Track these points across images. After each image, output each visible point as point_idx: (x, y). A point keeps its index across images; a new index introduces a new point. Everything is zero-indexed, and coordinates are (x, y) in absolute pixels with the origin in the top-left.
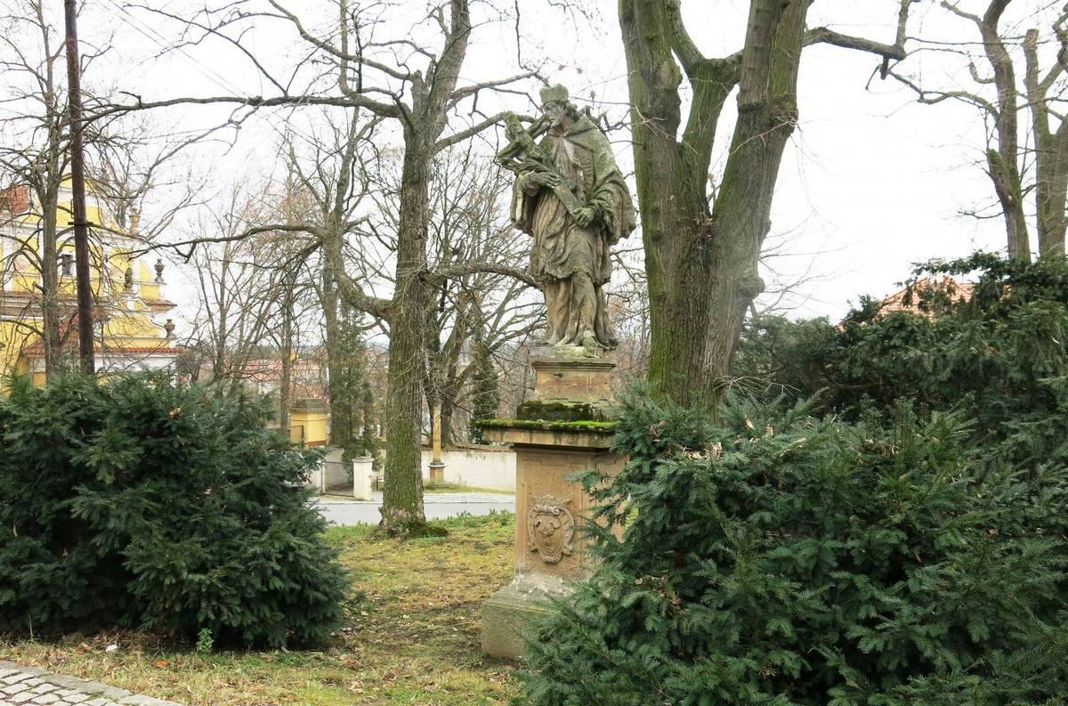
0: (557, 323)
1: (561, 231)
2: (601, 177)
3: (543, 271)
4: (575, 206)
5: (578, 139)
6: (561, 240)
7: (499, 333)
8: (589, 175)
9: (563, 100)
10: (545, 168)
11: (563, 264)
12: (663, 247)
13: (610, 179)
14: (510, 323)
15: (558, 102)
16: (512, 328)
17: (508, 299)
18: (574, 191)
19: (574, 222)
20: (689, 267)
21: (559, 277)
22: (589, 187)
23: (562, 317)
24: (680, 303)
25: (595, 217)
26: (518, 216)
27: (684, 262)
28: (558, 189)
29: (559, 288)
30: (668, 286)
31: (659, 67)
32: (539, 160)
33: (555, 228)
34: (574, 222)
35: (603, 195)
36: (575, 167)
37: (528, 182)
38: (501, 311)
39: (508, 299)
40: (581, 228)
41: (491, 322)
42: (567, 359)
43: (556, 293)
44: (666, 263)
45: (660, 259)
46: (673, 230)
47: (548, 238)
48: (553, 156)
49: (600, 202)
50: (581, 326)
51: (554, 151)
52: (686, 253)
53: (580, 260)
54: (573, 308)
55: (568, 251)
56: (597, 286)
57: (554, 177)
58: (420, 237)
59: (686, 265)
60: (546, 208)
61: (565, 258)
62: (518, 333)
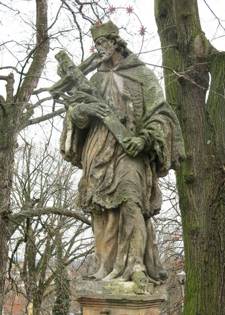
0: (105, 255)
1: (110, 162)
2: (150, 108)
3: (91, 200)
4: (125, 135)
5: (128, 73)
6: (110, 170)
7: (71, 255)
8: (138, 107)
9: (113, 34)
10: (95, 99)
11: (111, 194)
12: (196, 189)
13: (160, 110)
14: (78, 248)
15: (108, 37)
16: (79, 252)
17: (77, 234)
18: (124, 122)
19: (123, 152)
20: (219, 206)
21: (108, 207)
22: (138, 118)
23: (110, 249)
24: (212, 237)
25: (146, 146)
26: (68, 146)
27: (214, 202)
28: (107, 119)
29: (107, 219)
30: (200, 222)
31: (192, 39)
32: (89, 92)
33: (105, 158)
34: (123, 152)
35: (153, 125)
36: (125, 99)
37: (77, 112)
38: (72, 242)
39: (77, 234)
40: (131, 157)
41: (66, 248)
42: (115, 295)
43: (104, 224)
44: (199, 202)
45: (193, 199)
46: (204, 175)
47: (96, 167)
48: (102, 90)
49: (151, 131)
50: (130, 259)
51: (104, 84)
52: (216, 194)
53: (130, 190)
54: (122, 240)
55: (117, 181)
56: (146, 218)
57: (104, 107)
58: (6, 187)
59: (216, 204)
60: (95, 139)
61: (113, 188)
62: (82, 255)
